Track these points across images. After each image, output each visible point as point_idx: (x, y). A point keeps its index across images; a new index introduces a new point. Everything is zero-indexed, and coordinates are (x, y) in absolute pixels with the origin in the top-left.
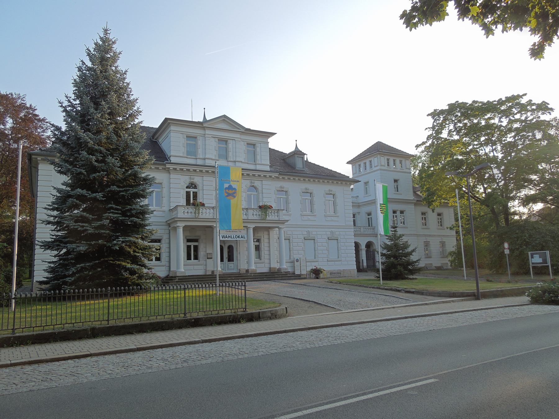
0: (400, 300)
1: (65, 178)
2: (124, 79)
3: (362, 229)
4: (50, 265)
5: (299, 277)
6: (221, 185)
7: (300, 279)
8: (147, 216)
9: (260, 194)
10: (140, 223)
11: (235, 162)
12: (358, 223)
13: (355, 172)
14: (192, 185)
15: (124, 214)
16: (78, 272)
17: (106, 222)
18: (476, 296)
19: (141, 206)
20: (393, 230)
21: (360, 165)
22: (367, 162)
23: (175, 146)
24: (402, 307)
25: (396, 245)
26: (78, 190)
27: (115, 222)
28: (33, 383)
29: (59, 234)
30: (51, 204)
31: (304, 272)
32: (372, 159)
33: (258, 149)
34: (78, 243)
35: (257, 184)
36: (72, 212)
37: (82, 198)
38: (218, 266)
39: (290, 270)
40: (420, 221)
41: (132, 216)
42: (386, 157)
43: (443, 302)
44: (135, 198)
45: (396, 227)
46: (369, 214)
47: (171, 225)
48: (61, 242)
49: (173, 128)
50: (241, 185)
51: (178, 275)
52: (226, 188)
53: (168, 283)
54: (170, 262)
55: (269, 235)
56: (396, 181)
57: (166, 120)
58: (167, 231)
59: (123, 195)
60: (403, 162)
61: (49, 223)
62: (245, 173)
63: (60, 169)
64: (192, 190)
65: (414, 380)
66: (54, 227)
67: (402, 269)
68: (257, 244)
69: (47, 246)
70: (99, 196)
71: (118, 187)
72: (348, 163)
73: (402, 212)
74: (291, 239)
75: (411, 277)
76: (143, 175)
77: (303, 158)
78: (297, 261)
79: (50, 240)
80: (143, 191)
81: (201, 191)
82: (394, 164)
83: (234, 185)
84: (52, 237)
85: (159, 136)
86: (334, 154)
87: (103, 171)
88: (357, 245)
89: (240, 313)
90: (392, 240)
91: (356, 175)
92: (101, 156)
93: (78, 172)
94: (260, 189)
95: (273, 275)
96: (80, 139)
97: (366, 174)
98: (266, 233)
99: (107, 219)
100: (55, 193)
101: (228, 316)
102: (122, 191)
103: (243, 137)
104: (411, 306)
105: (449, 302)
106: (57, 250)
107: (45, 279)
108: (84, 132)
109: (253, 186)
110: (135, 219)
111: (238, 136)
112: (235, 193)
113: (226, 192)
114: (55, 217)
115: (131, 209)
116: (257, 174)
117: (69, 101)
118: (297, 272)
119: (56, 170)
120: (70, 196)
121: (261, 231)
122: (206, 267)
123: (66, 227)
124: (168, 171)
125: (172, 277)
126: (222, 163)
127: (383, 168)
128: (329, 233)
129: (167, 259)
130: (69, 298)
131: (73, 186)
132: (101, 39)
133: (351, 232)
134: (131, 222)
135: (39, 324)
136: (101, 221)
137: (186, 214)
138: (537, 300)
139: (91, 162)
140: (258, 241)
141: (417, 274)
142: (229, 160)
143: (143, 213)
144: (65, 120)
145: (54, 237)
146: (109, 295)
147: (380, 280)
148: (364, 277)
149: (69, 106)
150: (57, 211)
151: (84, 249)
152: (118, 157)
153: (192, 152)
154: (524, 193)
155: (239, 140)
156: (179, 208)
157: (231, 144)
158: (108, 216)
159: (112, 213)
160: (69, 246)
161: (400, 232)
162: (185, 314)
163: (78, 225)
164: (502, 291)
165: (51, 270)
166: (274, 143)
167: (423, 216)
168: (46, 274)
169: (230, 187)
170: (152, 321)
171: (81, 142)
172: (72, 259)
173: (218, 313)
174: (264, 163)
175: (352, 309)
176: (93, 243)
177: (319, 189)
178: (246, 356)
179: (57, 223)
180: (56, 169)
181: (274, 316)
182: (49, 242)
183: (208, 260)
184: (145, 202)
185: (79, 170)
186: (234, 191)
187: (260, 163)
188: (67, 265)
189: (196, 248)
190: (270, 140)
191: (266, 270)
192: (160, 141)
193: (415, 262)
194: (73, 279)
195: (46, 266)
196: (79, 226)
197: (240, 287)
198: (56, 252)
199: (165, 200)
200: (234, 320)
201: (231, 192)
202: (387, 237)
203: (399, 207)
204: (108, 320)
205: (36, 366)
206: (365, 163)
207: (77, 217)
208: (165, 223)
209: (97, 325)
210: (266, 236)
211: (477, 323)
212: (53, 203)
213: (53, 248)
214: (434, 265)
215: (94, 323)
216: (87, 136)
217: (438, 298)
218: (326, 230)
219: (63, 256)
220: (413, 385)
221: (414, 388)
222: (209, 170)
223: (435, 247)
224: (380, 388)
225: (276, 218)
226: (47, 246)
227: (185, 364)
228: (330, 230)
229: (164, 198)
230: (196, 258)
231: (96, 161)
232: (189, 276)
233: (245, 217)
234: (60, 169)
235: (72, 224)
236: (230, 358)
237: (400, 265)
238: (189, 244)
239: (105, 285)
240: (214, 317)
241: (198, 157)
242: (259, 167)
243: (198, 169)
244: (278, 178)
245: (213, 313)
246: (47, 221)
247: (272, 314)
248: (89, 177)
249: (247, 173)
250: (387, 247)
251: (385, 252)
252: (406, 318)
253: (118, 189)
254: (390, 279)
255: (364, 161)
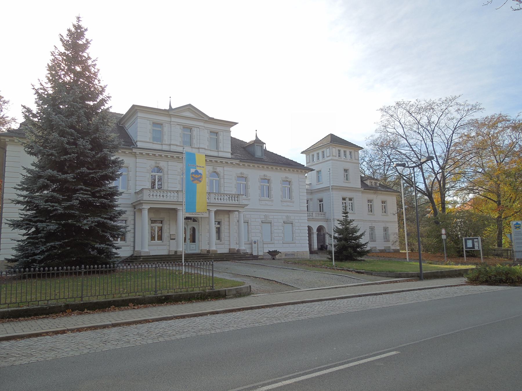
0: (352, 280)
1: (35, 159)
2: (95, 65)
3: (314, 215)
4: (19, 243)
5: (256, 258)
6: (188, 170)
7: (257, 259)
8: (115, 197)
9: (222, 180)
10: (109, 205)
11: (199, 148)
12: (311, 209)
13: (308, 161)
14: (159, 169)
15: (93, 195)
16: (47, 251)
17: (76, 202)
18: (420, 276)
19: (110, 188)
20: (344, 215)
21: (313, 155)
22: (320, 152)
23: (141, 133)
24: (355, 286)
25: (347, 229)
26: (49, 170)
27: (83, 203)
28: (14, 359)
29: (29, 213)
30: (20, 184)
31: (261, 253)
32: (324, 150)
33: (221, 137)
34: (48, 222)
35: (219, 169)
36: (42, 192)
37: (52, 179)
38: (182, 247)
39: (249, 251)
40: (366, 208)
41: (101, 197)
42: (337, 149)
43: (391, 282)
44: (103, 180)
45: (347, 213)
46: (321, 201)
47: (137, 207)
48: (30, 221)
49: (139, 114)
50: (205, 170)
51: (142, 255)
52: (193, 173)
53: (133, 262)
54: (134, 242)
55: (229, 218)
56: (346, 171)
57: (134, 106)
58: (132, 213)
59: (93, 177)
60: (353, 154)
61: (19, 202)
62: (209, 159)
63: (30, 150)
64: (157, 175)
65: (378, 352)
66: (23, 207)
67: (352, 252)
68: (218, 226)
69: (16, 225)
70: (70, 177)
71: (88, 168)
72: (302, 153)
73: (350, 199)
74: (250, 222)
75: (359, 258)
76: (112, 158)
77: (262, 147)
78: (255, 243)
79: (20, 219)
80: (113, 173)
81: (166, 176)
82: (345, 155)
83: (200, 170)
84: (20, 216)
85: (127, 119)
86: (289, 143)
87: (74, 153)
88: (310, 229)
89: (208, 291)
90: (343, 225)
91: (308, 165)
92: (72, 139)
93: (50, 153)
94: (222, 175)
95: (234, 256)
96: (51, 121)
97: (350, 162)
98: (227, 216)
99: (77, 199)
100: (25, 173)
101: (196, 293)
102: (92, 173)
103: (207, 125)
104: (362, 285)
105: (396, 282)
106: (26, 229)
107: (13, 257)
108: (56, 115)
109: (215, 172)
110: (104, 201)
111: (202, 124)
112: (201, 177)
113: (192, 177)
114: (25, 197)
115: (101, 191)
116: (219, 160)
117: (41, 85)
118: (255, 254)
119: (26, 151)
120: (40, 177)
121: (223, 213)
122: (170, 248)
123: (35, 207)
124: (135, 155)
125: (136, 256)
126: (188, 149)
127: (335, 158)
128: (285, 217)
129: (132, 240)
130: (39, 275)
131: (43, 167)
132: (74, 26)
133: (305, 217)
134: (102, 204)
135: (43, 298)
136: (71, 201)
137: (151, 197)
138: (475, 280)
139: (62, 144)
140: (219, 223)
141: (365, 256)
142: (193, 146)
143: (113, 193)
144: (36, 102)
145: (23, 216)
146: (83, 273)
147: (332, 261)
148: (316, 257)
149: (41, 89)
150: (27, 191)
151: (54, 228)
152: (88, 139)
153: (158, 137)
154: (458, 185)
155: (203, 128)
156: (145, 191)
157: (195, 132)
158: (78, 197)
159: (82, 193)
160: (40, 225)
161: (350, 217)
162: (156, 291)
163: (48, 205)
164: (442, 272)
165: (21, 249)
166: (236, 133)
167: (384, 204)
168: (15, 252)
169: (197, 172)
170: (124, 298)
171: (53, 125)
172: (41, 237)
173: (187, 291)
174: (226, 150)
175: (312, 287)
176: (63, 222)
177: (277, 176)
178: (218, 331)
179: (27, 202)
180: (26, 150)
181: (239, 294)
182: (18, 221)
183: (171, 241)
184: (113, 184)
185: (51, 151)
186: (199, 176)
187: (222, 150)
188: (37, 243)
189: (161, 229)
190: (232, 129)
191: (226, 251)
192: (126, 126)
193: (364, 245)
194: (42, 257)
195: (15, 244)
196: (49, 206)
197: (202, 267)
198: (24, 232)
199: (131, 183)
200: (203, 297)
201: (196, 176)
202: (339, 222)
203: (348, 195)
204: (82, 297)
205: (13, 342)
206: (318, 154)
207: (47, 197)
208: (131, 205)
209: (71, 301)
210: (227, 219)
211: (424, 301)
212: (23, 183)
213: (22, 226)
214: (378, 248)
215: (68, 300)
216: (59, 118)
217: (379, 278)
218: (282, 214)
219: (33, 235)
220: (379, 357)
221: (379, 359)
222: (175, 156)
223: (379, 233)
224: (348, 360)
225: (236, 202)
226: (16, 225)
227: (161, 339)
228: (286, 214)
229: (132, 179)
230: (160, 238)
231: (67, 143)
232: (153, 256)
233: (208, 201)
234: (30, 150)
235: (42, 204)
236: (203, 333)
237: (350, 247)
238: (153, 225)
239: (75, 263)
240: (184, 294)
241: (164, 143)
242: (221, 154)
243: (163, 154)
244: (239, 164)
245: (182, 290)
246: (17, 201)
247: (237, 292)
248: (60, 158)
249: (210, 159)
250: (338, 231)
251: (336, 235)
252: (360, 296)
253: (88, 171)
254: (341, 260)
255: (318, 152)
